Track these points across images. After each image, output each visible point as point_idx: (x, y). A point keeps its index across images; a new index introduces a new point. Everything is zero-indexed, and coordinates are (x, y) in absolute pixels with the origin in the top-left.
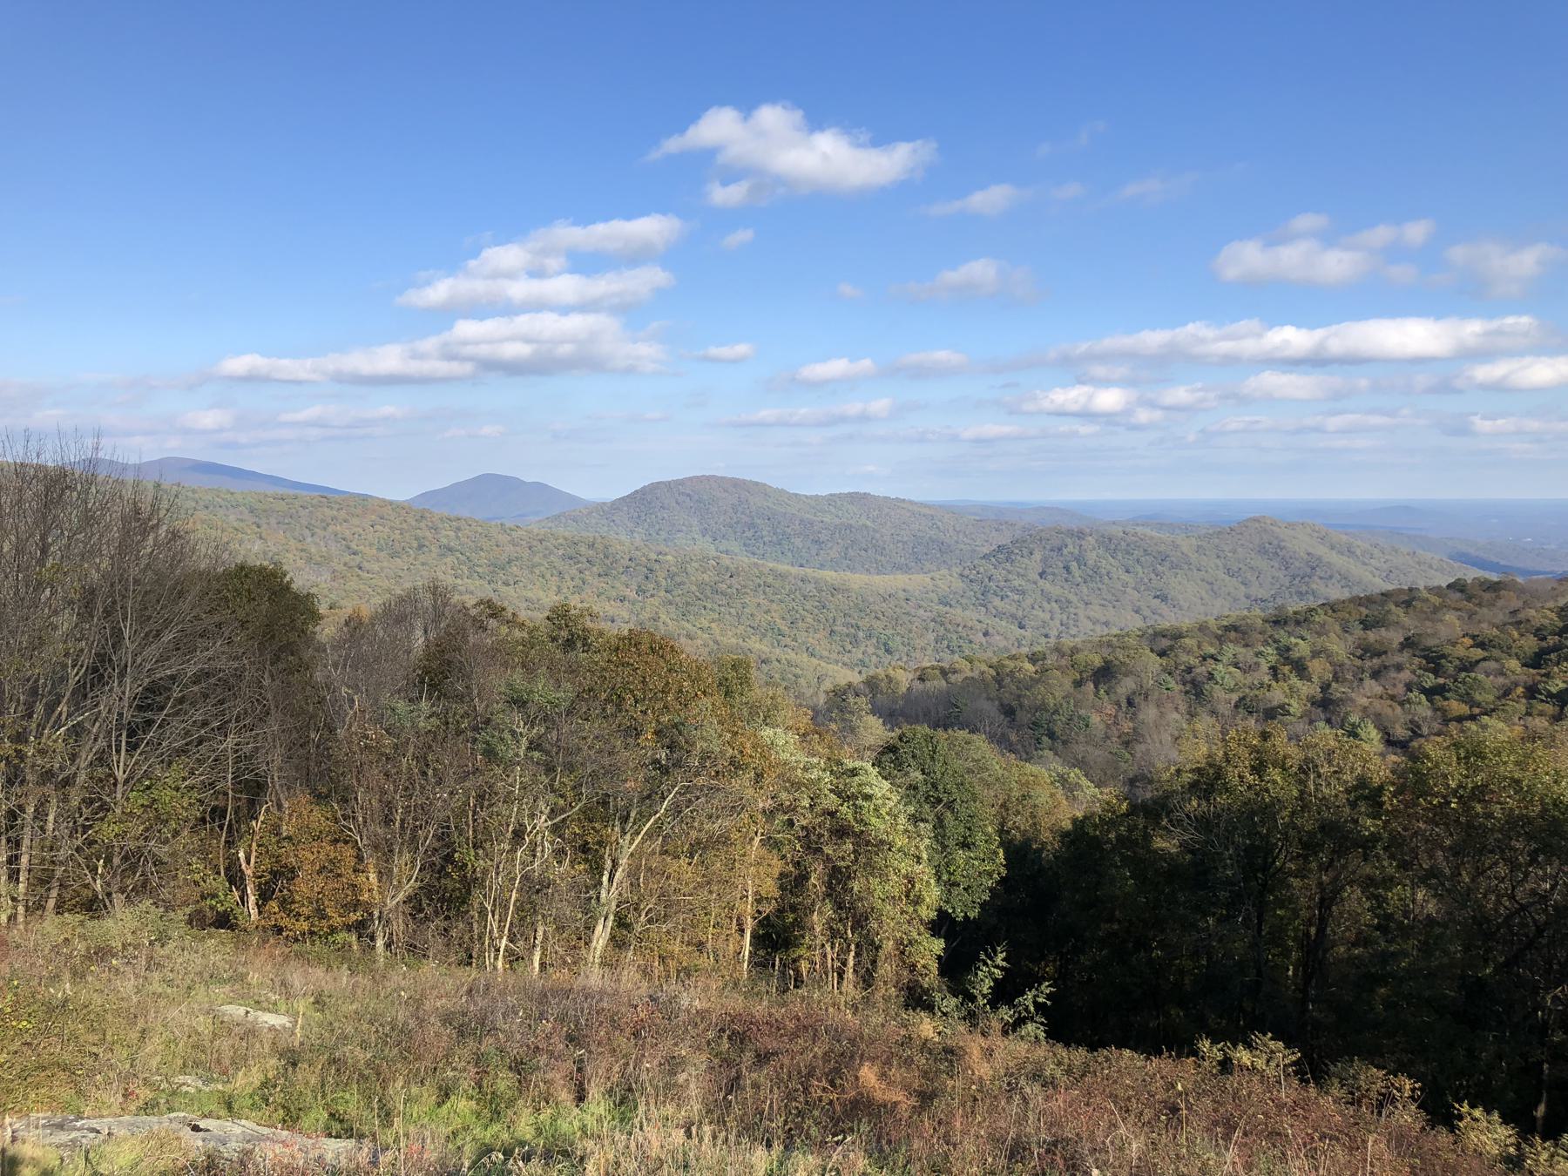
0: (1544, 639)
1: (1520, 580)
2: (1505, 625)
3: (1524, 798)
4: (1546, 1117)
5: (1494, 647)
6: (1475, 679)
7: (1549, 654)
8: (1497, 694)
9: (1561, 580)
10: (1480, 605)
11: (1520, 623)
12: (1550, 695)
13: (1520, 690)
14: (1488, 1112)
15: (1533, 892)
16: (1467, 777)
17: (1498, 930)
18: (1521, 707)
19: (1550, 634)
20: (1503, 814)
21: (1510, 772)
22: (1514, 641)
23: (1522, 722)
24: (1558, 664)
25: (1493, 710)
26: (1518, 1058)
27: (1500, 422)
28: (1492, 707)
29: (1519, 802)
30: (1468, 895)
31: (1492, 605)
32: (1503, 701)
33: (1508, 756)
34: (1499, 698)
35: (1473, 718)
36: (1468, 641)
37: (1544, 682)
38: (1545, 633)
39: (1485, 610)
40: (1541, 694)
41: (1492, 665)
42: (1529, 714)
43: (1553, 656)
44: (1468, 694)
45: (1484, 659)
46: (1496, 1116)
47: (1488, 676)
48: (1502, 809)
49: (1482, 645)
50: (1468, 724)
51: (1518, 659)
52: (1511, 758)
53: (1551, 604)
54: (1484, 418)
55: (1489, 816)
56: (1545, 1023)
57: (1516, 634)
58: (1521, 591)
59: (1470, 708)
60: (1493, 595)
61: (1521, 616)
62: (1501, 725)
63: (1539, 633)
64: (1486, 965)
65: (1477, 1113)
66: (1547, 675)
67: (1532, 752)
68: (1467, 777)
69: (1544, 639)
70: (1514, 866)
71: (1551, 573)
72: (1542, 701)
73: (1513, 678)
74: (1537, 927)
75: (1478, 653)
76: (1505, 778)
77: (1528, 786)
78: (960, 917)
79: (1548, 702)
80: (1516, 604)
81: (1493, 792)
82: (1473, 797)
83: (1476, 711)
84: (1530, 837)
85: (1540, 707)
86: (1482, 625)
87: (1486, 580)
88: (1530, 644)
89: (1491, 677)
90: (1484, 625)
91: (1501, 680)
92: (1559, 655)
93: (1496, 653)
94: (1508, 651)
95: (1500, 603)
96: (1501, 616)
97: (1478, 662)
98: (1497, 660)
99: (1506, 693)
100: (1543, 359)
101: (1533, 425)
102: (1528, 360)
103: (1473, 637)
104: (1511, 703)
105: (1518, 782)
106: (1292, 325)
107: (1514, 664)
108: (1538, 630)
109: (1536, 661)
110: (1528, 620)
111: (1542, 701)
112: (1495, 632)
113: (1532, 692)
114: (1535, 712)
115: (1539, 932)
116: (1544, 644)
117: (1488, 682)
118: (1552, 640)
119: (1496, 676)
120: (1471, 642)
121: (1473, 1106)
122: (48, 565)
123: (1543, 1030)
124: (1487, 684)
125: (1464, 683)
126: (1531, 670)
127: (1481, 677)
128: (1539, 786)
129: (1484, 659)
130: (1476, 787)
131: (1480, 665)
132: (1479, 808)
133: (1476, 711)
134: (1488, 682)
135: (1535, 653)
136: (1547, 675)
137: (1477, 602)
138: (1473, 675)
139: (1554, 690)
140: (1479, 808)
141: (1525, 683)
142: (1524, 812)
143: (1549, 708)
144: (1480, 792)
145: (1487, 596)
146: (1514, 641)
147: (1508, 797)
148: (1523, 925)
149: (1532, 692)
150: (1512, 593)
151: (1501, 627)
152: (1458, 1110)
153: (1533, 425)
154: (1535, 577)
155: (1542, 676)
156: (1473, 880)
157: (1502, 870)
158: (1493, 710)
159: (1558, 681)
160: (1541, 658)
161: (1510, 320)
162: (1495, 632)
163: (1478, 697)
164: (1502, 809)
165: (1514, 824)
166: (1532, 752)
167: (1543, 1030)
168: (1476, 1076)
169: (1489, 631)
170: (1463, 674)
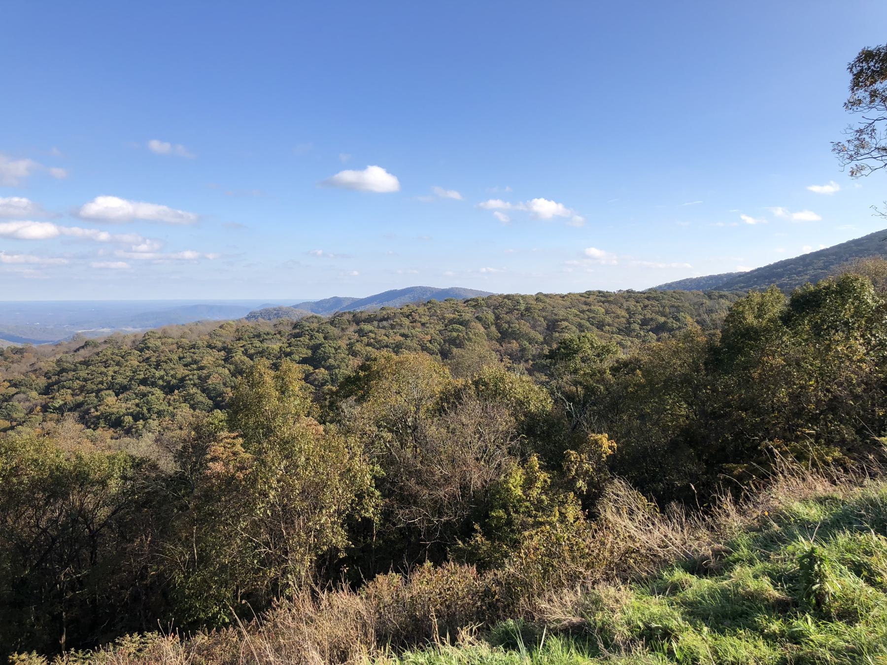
0: (49, 378)
1: (34, 346)
2: (27, 372)
3: (40, 469)
4: (66, 642)
5: (22, 385)
6: (12, 405)
7: (53, 386)
8: (26, 412)
9: (57, 345)
10: (12, 362)
11: (36, 370)
12: (55, 409)
13: (39, 408)
14: (30, 653)
15: (49, 520)
16: (6, 463)
17: (31, 547)
18: (40, 417)
19: (53, 375)
20: (29, 481)
21: (31, 456)
22: (33, 381)
23: (41, 426)
24: (58, 391)
25: (24, 422)
26: (48, 615)
27: (15, 257)
28: (23, 420)
29: (37, 471)
30: (13, 532)
31: (19, 362)
32: (30, 416)
33: (30, 447)
34: (27, 414)
35: (12, 428)
36: (7, 384)
37: (52, 402)
38: (50, 375)
39: (15, 365)
40: (51, 409)
41: (22, 396)
42: (44, 421)
43: (55, 387)
44: (9, 414)
45: (17, 393)
46: (34, 653)
47: (20, 403)
48: (28, 478)
49: (15, 385)
50: (10, 432)
51: (36, 390)
52: (32, 448)
53: (51, 359)
54: (6, 254)
55: (21, 483)
56: (61, 590)
57: (34, 377)
58: (36, 353)
59: (11, 422)
60: (20, 356)
61: (36, 367)
62: (28, 430)
63: (47, 375)
64: (25, 569)
65: (23, 656)
66: (53, 398)
67: (43, 442)
68: (6, 463)
69: (49, 378)
70: (37, 508)
71: (52, 341)
72: (51, 412)
73: (34, 402)
74: (52, 539)
75: (13, 390)
76: (28, 460)
77: (42, 461)
78: (34, 653)
79: (54, 413)
80: (34, 360)
81: (22, 469)
82: (11, 474)
83: (14, 424)
84: (44, 490)
85: (50, 416)
86: (14, 374)
87: (15, 348)
88: (42, 382)
89: (22, 403)
90: (16, 374)
91: (27, 404)
92: (59, 386)
93: (23, 389)
94: (30, 387)
95: (23, 360)
96: (25, 367)
97: (13, 395)
98: (24, 393)
99: (31, 411)
100: (37, 222)
101: (35, 259)
102: (29, 222)
103: (10, 381)
104: (34, 416)
105: (36, 460)
106: (379, 166)
107: (34, 394)
108: (46, 373)
109: (47, 391)
110: (40, 369)
111: (51, 412)
112: (22, 377)
113: (45, 408)
114: (48, 419)
115: (54, 540)
116: (50, 381)
117: (20, 406)
118: (54, 378)
119: (24, 402)
120: (9, 384)
121: (20, 653)
122: (852, 375)
123: (60, 594)
124: (19, 408)
125: (6, 408)
126: (44, 396)
127: (16, 404)
128: (48, 460)
129: (17, 393)
130: (13, 468)
131: (15, 397)
132: (14, 480)
133: (14, 424)
134: (20, 406)
135: (46, 386)
136: (53, 398)
137: (10, 361)
138: (11, 403)
139: (57, 406)
140: (14, 480)
141: (41, 403)
142: (41, 477)
143: (55, 416)
144: (15, 471)
145: (16, 357)
146: (33, 381)
147: (31, 470)
148: (46, 539)
149: (45, 408)
150: (30, 354)
151: (26, 374)
152: (12, 659)
153: (35, 259)
154: (43, 344)
155: (50, 399)
156: (14, 523)
157: (30, 512)
158: (24, 422)
159: (59, 400)
160: (49, 389)
161: (16, 199)
162: (22, 377)
163: (15, 416)
164: (28, 478)
165: (36, 485)
166: (43, 442)
167: (60, 594)
168: (25, 634)
169: (19, 377)
170: (6, 403)
